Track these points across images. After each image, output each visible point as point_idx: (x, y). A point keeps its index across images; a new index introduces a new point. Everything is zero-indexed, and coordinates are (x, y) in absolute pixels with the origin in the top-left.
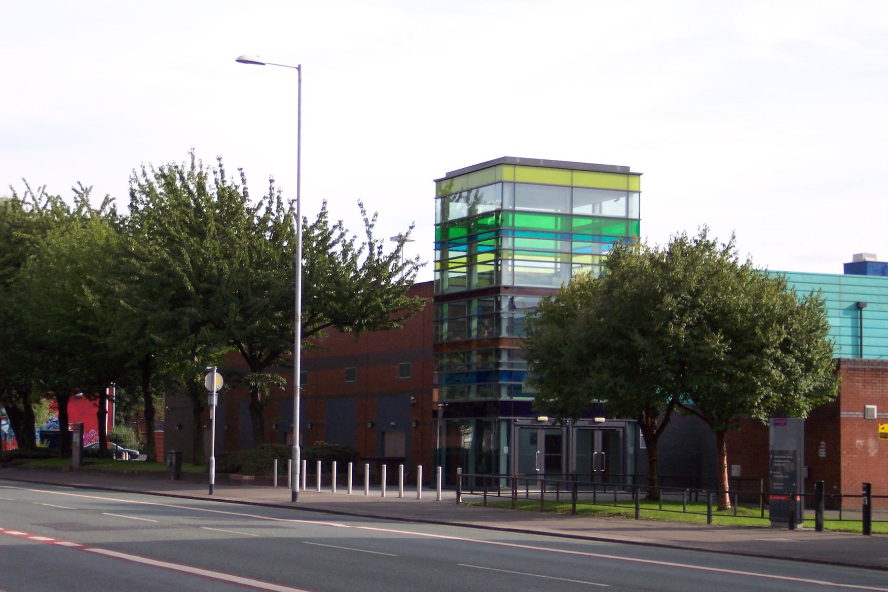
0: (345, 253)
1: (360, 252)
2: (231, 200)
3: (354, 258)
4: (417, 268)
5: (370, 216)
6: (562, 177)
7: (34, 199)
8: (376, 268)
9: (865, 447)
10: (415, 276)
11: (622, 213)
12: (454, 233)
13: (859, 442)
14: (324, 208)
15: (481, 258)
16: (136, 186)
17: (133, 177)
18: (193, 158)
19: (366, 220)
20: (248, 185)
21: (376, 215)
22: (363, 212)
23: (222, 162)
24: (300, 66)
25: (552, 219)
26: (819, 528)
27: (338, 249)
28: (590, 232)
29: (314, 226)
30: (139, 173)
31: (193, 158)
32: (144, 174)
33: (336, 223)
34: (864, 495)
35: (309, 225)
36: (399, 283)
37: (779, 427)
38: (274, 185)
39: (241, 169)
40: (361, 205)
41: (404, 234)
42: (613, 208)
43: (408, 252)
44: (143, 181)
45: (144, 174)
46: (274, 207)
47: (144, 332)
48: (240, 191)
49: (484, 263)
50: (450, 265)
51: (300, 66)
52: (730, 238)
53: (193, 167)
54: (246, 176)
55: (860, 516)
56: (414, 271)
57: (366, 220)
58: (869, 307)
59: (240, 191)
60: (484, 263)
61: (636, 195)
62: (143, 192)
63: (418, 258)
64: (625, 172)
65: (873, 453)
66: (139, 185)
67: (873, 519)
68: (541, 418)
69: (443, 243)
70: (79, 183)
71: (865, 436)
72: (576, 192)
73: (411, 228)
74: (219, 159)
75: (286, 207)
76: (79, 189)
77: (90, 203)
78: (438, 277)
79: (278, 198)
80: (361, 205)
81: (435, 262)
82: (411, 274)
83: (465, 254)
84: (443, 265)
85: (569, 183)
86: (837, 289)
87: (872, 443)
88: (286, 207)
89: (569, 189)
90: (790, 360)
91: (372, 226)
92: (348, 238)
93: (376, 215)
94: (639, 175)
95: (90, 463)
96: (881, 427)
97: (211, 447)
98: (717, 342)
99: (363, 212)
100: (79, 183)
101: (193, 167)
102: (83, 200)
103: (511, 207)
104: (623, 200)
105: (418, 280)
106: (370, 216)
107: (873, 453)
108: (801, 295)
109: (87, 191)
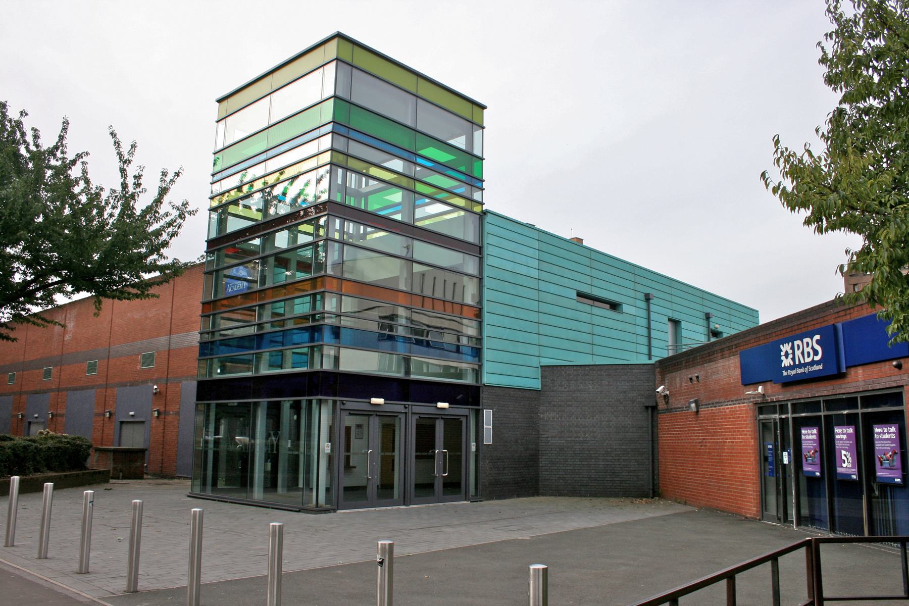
4: (182, 216)
6: (409, 82)
19: (120, 155)
21: (133, 146)
22: (117, 144)
40: (113, 134)
41: (834, 27)
43: (174, 197)
57: (120, 155)
63: (185, 204)
93: (133, 146)
94: (483, 107)
99: (117, 144)
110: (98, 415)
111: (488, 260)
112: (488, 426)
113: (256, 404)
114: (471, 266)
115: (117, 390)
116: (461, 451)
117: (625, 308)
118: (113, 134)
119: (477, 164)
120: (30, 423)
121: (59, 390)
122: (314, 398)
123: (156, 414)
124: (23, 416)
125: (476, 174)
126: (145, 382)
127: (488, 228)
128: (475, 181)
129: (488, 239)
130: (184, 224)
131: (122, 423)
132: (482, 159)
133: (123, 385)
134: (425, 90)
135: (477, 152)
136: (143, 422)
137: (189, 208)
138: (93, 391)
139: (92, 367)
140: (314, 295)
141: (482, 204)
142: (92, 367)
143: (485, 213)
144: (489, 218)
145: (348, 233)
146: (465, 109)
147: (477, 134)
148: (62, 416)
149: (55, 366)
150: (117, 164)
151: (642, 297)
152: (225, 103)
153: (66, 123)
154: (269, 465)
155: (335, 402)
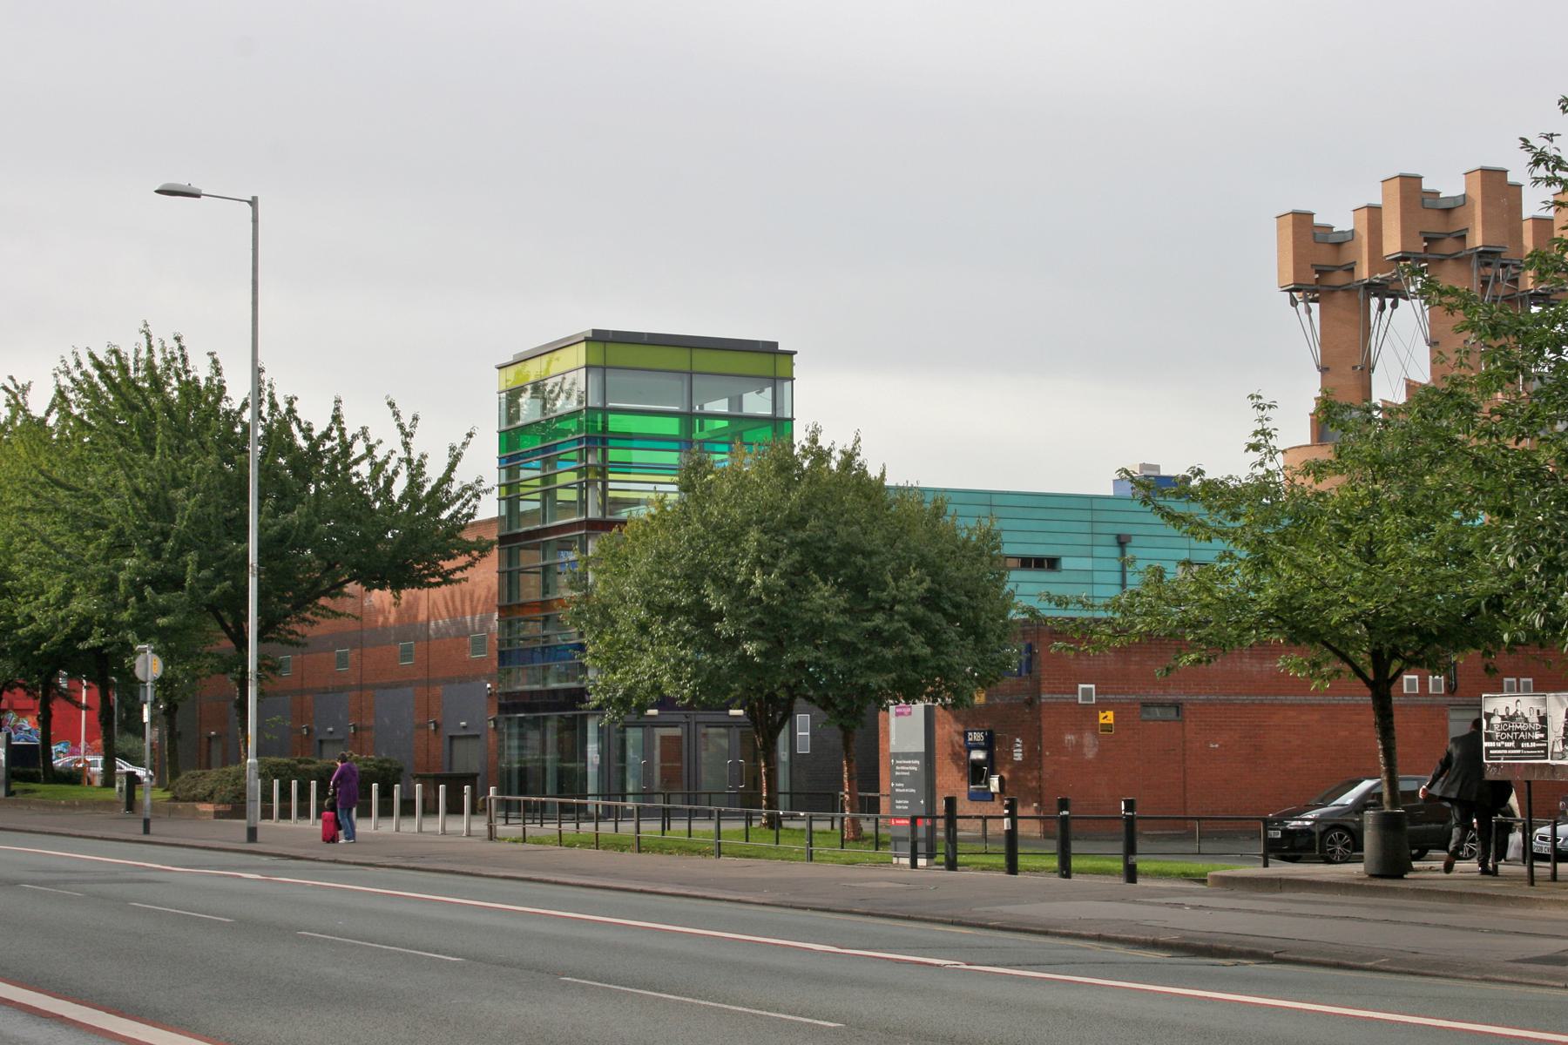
0: (374, 477)
1: (396, 473)
2: (203, 399)
3: (389, 482)
4: (477, 496)
6: (679, 359)
9: (1079, 746)
11: (767, 411)
12: (528, 443)
13: (1070, 738)
14: (337, 409)
15: (562, 479)
16: (65, 381)
17: (62, 368)
18: (148, 336)
19: (401, 426)
21: (415, 419)
22: (397, 415)
23: (183, 343)
25: (675, 421)
26: (1448, 868)
27: (364, 469)
28: (725, 439)
29: (326, 435)
30: (72, 364)
31: (148, 336)
32: (79, 364)
33: (357, 430)
34: (1007, 816)
35: (316, 434)
36: (452, 517)
37: (901, 718)
39: (211, 354)
40: (392, 405)
41: (849, 448)
42: (757, 403)
43: (462, 477)
44: (77, 374)
45: (79, 364)
46: (265, 408)
49: (566, 487)
52: (463, 438)
53: (150, 350)
54: (222, 364)
55: (1002, 848)
57: (401, 426)
58: (1135, 541)
60: (566, 487)
61: (787, 385)
63: (479, 482)
64: (770, 349)
65: (1090, 754)
66: (73, 380)
67: (1020, 850)
68: (732, 712)
69: (511, 460)
70: (11, 378)
71: (1079, 731)
72: (697, 381)
73: (470, 435)
75: (283, 407)
76: (11, 387)
77: (29, 407)
79: (271, 395)
83: (538, 473)
84: (511, 493)
85: (686, 367)
86: (1087, 516)
87: (1088, 739)
88: (283, 407)
89: (686, 377)
90: (937, 619)
92: (380, 453)
93: (415, 419)
94: (792, 353)
95: (27, 791)
96: (1102, 715)
98: (823, 596)
99: (397, 415)
100: (11, 378)
101: (150, 350)
102: (18, 403)
103: (599, 404)
104: (768, 391)
106: (406, 420)
107: (1090, 754)
108: (966, 525)
109: (25, 390)
110: (419, 727)
115: (439, 690)
116: (662, 768)
117: (1065, 563)
118: (392, 405)
120: (321, 742)
121: (361, 687)
123: (492, 725)
124: (309, 730)
126: (476, 678)
131: (452, 738)
132: (792, 419)
133: (449, 681)
134: (703, 360)
136: (477, 736)
138: (410, 690)
139: (406, 654)
142: (406, 654)
146: (761, 364)
148: (369, 728)
149: (353, 648)
150: (399, 438)
151: (1112, 540)
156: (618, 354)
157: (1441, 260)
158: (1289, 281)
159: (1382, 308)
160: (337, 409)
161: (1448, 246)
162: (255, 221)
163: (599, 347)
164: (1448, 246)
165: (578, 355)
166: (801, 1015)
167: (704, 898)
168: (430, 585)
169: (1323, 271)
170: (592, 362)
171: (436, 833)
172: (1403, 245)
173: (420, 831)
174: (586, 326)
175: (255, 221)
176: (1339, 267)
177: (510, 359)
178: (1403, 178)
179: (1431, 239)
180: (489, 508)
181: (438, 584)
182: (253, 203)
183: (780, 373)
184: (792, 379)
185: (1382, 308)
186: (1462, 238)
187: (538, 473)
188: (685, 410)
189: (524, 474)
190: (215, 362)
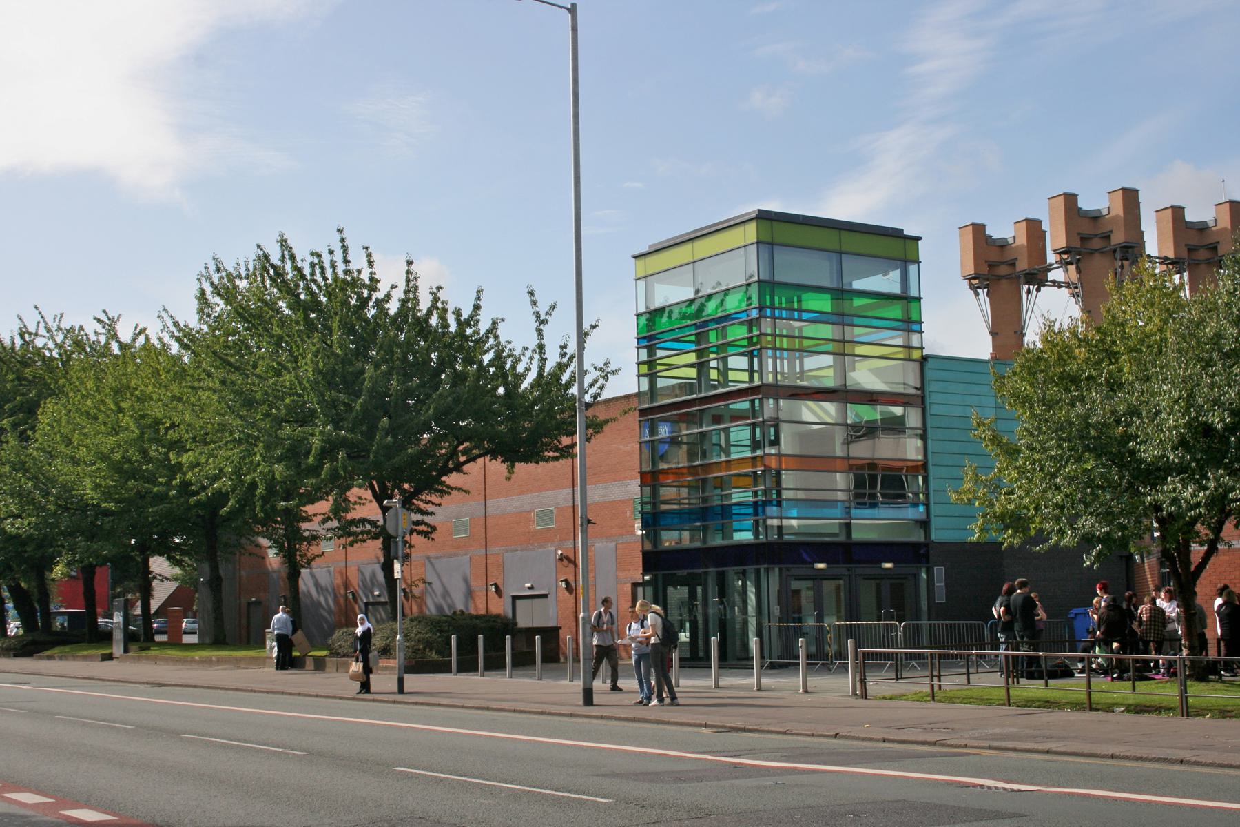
4: (606, 377)
5: (543, 308)
7: (49, 331)
8: (550, 384)
10: (601, 388)
11: (897, 289)
19: (538, 314)
20: (376, 268)
22: (534, 303)
24: (574, 5)
30: (212, 268)
38: (413, 268)
40: (531, 293)
47: (267, 471)
48: (365, 276)
50: (659, 368)
51: (574, 5)
54: (374, 258)
56: (601, 381)
57: (538, 314)
59: (365, 276)
62: (217, 292)
63: (606, 364)
69: (649, 340)
74: (340, 231)
78: (645, 386)
80: (531, 293)
81: (639, 363)
82: (598, 385)
84: (650, 368)
85: (837, 248)
91: (544, 322)
93: (553, 307)
97: (1194, 807)
99: (534, 303)
105: (606, 395)
106: (543, 308)
111: (933, 410)
112: (940, 584)
113: (706, 573)
114: (913, 418)
119: (914, 305)
122: (762, 568)
125: (914, 317)
127: (929, 374)
128: (911, 324)
129: (931, 387)
130: (608, 384)
131: (515, 598)
132: (919, 299)
134: (850, 242)
135: (913, 292)
136: (545, 596)
137: (612, 367)
140: (751, 352)
141: (922, 348)
143: (924, 359)
144: (930, 364)
145: (782, 373)
147: (912, 268)
152: (641, 262)
153: (479, 292)
154: (647, 490)
155: (780, 570)
156: (784, 232)
157: (1092, 252)
158: (971, 270)
159: (1028, 292)
160: (479, 299)
161: (1096, 244)
162: (575, 29)
163: (767, 224)
164: (1096, 244)
165: (750, 232)
166: (546, 788)
167: (439, 705)
168: (547, 460)
169: (992, 266)
170: (762, 239)
171: (710, 687)
172: (1067, 242)
173: (717, 686)
174: (751, 208)
175: (575, 29)
176: (1003, 263)
177: (646, 249)
178: (974, 225)
179: (1084, 239)
180: (627, 383)
181: (557, 459)
182: (573, 10)
183: (909, 257)
184: (919, 262)
185: (1028, 292)
186: (1013, 264)
187: (693, 347)
188: (834, 285)
189: (659, 353)
190: (369, 255)
